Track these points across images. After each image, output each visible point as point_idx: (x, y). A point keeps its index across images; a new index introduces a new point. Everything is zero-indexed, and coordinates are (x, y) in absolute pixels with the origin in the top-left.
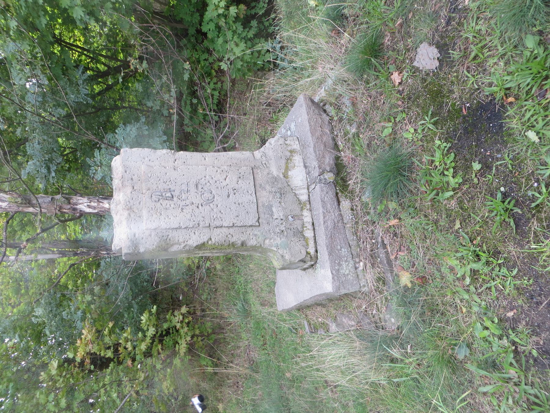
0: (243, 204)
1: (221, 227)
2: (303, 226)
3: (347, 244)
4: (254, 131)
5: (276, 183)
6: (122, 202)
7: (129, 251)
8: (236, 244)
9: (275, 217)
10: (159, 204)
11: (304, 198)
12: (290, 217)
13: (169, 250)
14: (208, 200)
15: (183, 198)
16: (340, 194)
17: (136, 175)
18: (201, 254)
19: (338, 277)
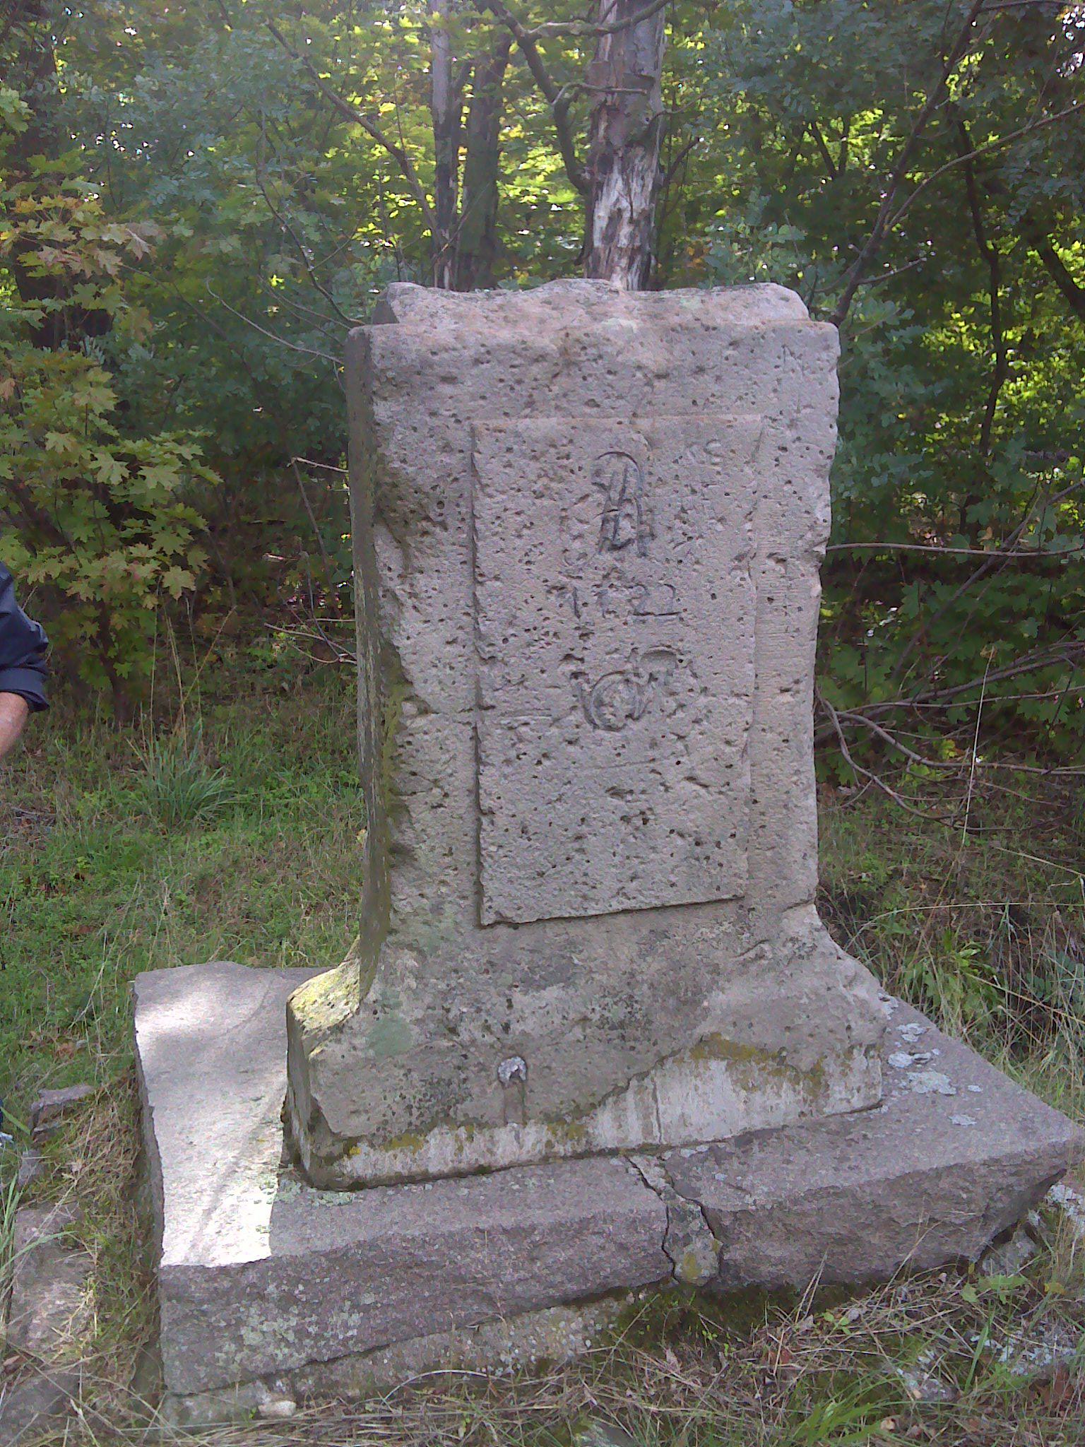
0: (578, 857)
1: (478, 760)
2: (478, 1124)
3: (383, 1339)
4: (905, 865)
5: (671, 1002)
6: (597, 328)
7: (377, 352)
8: (398, 823)
9: (517, 996)
10: (587, 488)
11: (605, 1129)
12: (517, 1064)
13: (381, 530)
14: (600, 704)
15: (612, 594)
16: (615, 1306)
17: (715, 388)
18: (364, 664)
19: (227, 1292)
